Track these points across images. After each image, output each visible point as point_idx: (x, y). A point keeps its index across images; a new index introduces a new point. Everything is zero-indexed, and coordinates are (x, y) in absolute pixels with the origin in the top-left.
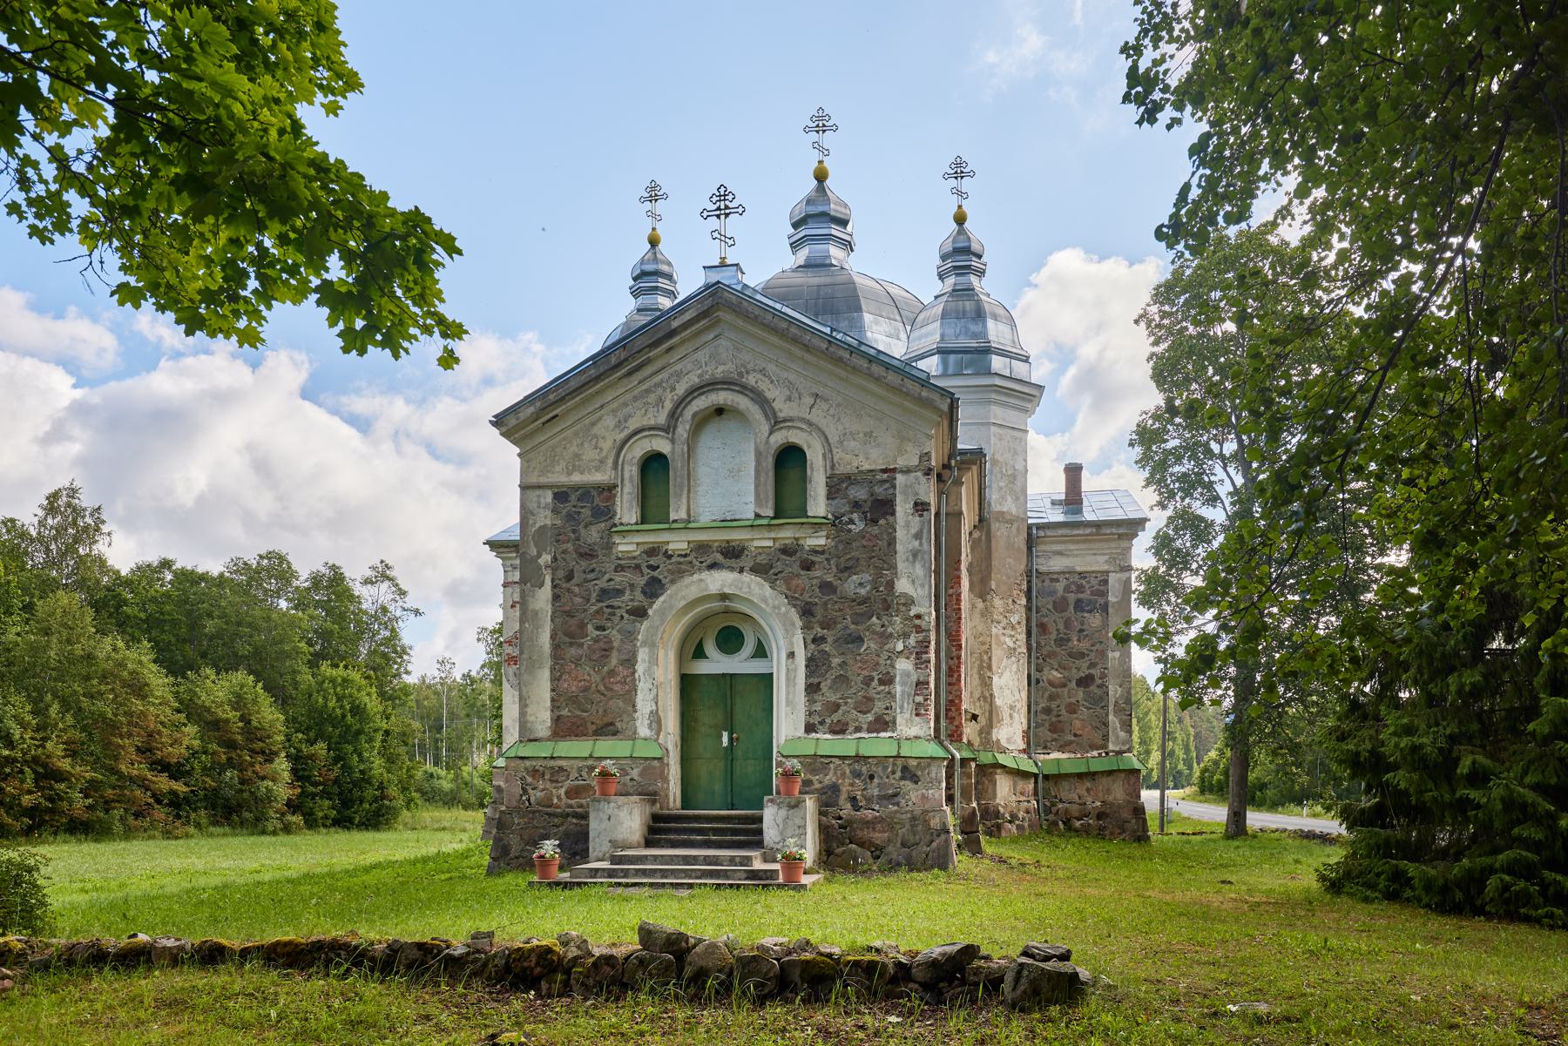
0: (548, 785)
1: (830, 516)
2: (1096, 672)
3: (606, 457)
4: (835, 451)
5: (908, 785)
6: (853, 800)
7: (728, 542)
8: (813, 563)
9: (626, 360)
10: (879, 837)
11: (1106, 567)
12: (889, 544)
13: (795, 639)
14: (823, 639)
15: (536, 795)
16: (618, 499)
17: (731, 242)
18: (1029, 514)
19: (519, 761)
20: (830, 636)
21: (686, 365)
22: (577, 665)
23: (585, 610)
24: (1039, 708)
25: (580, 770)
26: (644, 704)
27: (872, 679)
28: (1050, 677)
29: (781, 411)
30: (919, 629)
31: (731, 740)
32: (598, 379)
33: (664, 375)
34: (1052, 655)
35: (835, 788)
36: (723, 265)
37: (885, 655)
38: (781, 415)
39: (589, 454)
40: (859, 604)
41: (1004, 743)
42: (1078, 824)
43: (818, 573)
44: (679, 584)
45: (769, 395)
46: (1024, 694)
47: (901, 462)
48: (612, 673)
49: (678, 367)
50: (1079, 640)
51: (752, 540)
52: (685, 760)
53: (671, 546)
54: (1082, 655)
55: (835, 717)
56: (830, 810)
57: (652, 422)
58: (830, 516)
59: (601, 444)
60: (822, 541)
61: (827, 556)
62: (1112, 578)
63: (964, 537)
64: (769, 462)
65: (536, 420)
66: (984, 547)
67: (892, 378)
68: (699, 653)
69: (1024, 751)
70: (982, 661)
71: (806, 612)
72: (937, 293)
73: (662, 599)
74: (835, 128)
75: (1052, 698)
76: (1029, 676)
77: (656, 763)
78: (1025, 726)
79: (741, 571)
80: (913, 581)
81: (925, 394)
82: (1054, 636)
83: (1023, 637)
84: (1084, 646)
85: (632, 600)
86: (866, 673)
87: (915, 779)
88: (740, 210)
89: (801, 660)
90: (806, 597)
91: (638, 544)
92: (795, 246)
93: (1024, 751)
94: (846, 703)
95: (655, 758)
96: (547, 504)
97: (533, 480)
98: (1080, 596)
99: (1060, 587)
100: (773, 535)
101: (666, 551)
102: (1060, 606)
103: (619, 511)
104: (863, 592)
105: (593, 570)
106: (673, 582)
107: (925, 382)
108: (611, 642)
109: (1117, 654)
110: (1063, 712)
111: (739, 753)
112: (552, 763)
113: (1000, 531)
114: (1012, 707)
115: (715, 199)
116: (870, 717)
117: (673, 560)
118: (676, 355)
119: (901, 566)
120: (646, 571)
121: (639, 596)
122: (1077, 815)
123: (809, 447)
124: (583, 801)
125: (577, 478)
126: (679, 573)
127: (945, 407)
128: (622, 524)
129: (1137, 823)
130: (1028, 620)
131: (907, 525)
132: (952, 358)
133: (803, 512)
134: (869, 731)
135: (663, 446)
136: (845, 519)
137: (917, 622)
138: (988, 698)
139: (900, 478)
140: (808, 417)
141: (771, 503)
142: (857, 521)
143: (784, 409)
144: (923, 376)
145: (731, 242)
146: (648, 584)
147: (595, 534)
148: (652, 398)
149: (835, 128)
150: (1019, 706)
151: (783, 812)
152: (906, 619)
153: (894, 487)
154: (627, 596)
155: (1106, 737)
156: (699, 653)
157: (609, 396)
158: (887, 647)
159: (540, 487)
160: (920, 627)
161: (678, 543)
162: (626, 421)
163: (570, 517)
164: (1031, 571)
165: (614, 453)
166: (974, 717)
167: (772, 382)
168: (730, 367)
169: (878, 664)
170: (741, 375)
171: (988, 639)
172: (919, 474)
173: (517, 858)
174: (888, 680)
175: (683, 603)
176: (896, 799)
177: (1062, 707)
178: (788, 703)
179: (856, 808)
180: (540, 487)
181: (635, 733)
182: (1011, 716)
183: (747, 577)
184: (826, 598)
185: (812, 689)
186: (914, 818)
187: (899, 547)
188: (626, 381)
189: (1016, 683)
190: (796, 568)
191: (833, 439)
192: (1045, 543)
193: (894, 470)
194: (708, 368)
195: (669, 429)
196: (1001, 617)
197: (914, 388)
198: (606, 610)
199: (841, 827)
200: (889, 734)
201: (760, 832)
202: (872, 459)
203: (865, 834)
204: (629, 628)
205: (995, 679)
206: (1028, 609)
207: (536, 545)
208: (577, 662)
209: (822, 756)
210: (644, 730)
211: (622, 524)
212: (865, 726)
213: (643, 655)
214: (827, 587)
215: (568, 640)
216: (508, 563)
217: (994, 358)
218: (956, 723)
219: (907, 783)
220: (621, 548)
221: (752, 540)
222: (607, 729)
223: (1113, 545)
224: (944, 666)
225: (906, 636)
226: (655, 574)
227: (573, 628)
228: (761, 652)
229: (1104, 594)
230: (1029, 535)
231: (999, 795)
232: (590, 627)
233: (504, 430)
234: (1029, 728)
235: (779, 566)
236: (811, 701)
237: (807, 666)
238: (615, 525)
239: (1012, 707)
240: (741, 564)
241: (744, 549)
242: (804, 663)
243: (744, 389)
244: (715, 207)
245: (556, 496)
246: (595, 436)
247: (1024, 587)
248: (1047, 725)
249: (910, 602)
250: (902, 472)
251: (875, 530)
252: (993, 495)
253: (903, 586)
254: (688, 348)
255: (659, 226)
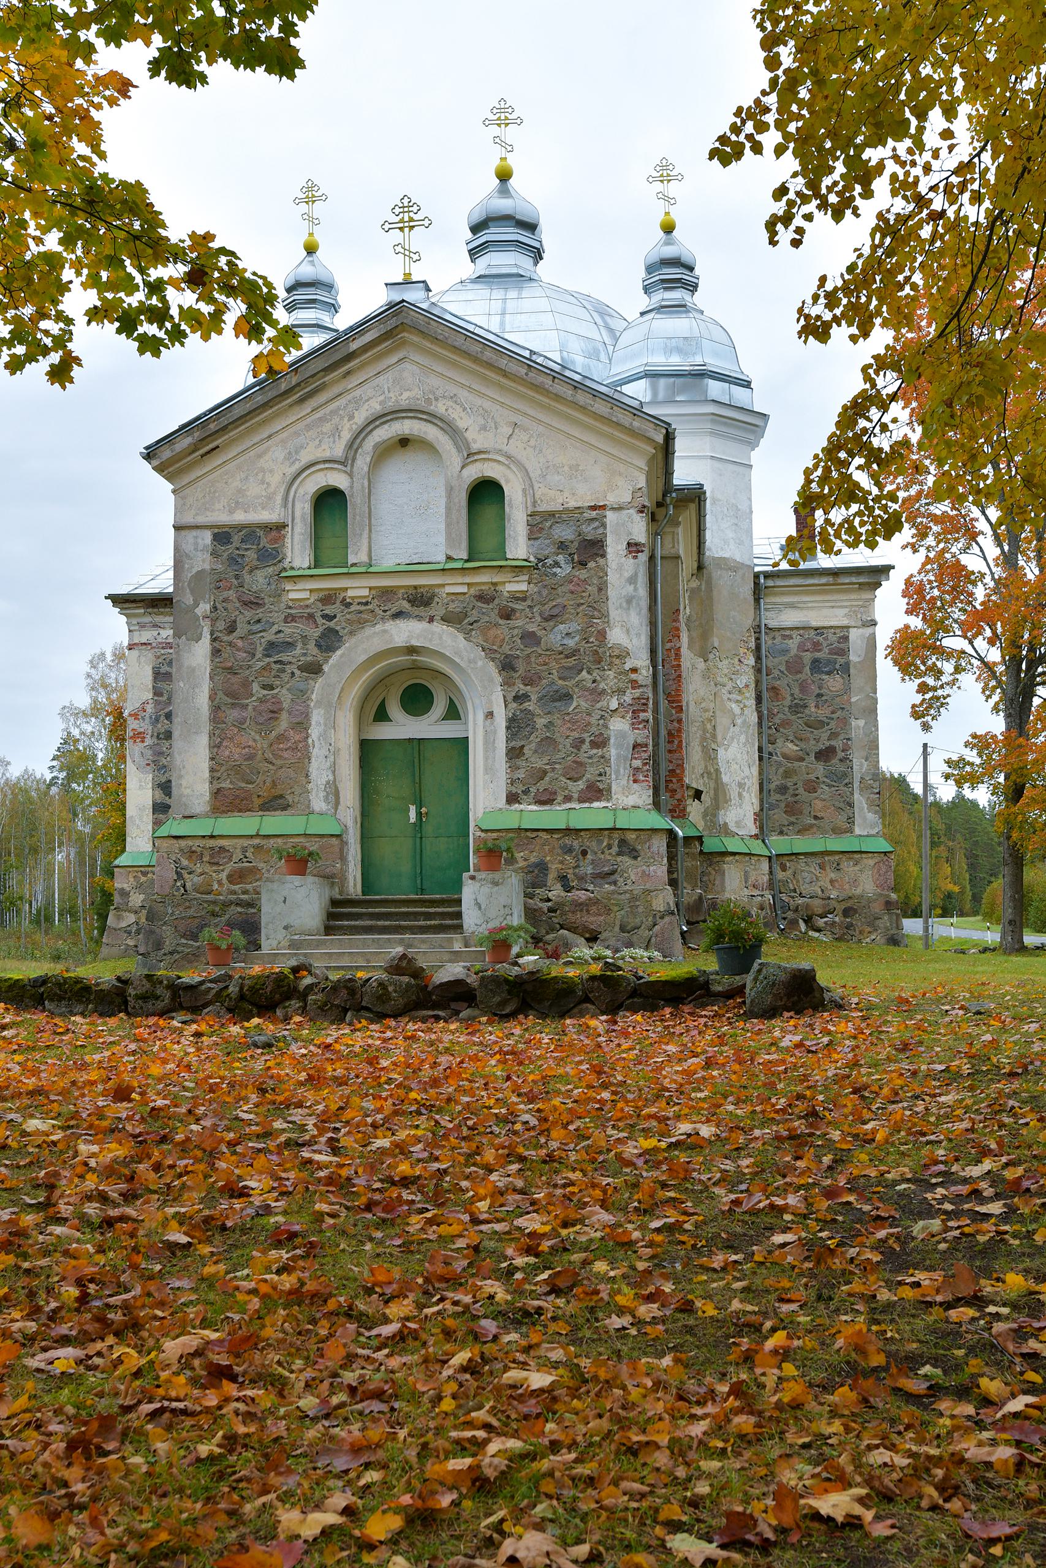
0: (208, 868)
1: (532, 559)
2: (838, 743)
3: (274, 493)
4: (536, 486)
5: (626, 860)
6: (563, 879)
7: (415, 587)
8: (513, 610)
9: (298, 385)
10: (593, 921)
11: (845, 622)
12: (600, 590)
13: (493, 698)
14: (525, 697)
15: (192, 881)
16: (288, 540)
17: (415, 257)
18: (756, 561)
19: (174, 841)
20: (534, 693)
21: (367, 390)
22: (240, 729)
23: (250, 667)
24: (773, 786)
25: (244, 850)
26: (319, 772)
27: (583, 741)
28: (785, 750)
29: (475, 441)
30: (635, 685)
31: (419, 815)
32: (266, 405)
33: (341, 402)
34: (786, 723)
35: (542, 867)
36: (408, 282)
37: (597, 715)
38: (475, 447)
39: (254, 490)
40: (567, 657)
41: (732, 827)
42: (821, 922)
43: (519, 623)
44: (359, 636)
45: (461, 424)
46: (755, 770)
47: (611, 499)
48: (281, 738)
49: (358, 393)
50: (817, 706)
51: (443, 586)
52: (366, 837)
53: (350, 593)
54: (821, 724)
55: (542, 785)
56: (538, 891)
57: (327, 454)
58: (532, 559)
59: (268, 478)
60: (523, 587)
61: (529, 602)
62: (854, 634)
63: (682, 586)
64: (462, 498)
65: (193, 452)
66: (704, 598)
67: (601, 408)
68: (381, 715)
69: (756, 837)
70: (705, 731)
71: (507, 666)
72: (643, 309)
73: (339, 652)
74: (519, 122)
75: (787, 774)
76: (760, 750)
77: (334, 840)
78: (757, 808)
79: (431, 620)
80: (628, 631)
81: (636, 424)
82: (787, 702)
83: (752, 702)
84: (823, 713)
85: (305, 654)
86: (575, 734)
87: (634, 854)
88: (426, 223)
89: (501, 722)
90: (506, 649)
91: (311, 591)
92: (474, 253)
93: (756, 837)
94: (553, 769)
95: (332, 836)
96: (205, 546)
97: (188, 519)
98: (818, 655)
99: (793, 644)
100: (468, 580)
101: (344, 599)
102: (794, 667)
103: (289, 554)
104: (571, 643)
105: (259, 621)
106: (352, 633)
107: (637, 412)
108: (280, 703)
109: (861, 723)
110: (801, 791)
111: (428, 829)
112: (212, 843)
113: (722, 581)
114: (741, 785)
115: (397, 210)
116: (581, 785)
117: (353, 608)
118: (355, 380)
119: (614, 614)
120: (320, 621)
121: (312, 649)
122: (820, 911)
123: (507, 481)
124: (249, 887)
125: (240, 517)
126: (360, 623)
127: (660, 438)
128: (292, 568)
129: (890, 920)
130: (758, 683)
131: (620, 568)
132: (662, 382)
133: (500, 551)
134: (581, 800)
135: (339, 480)
136: (549, 561)
137: (633, 676)
138: (714, 774)
139: (611, 517)
140: (505, 448)
141: (464, 544)
142: (562, 563)
143: (478, 440)
144: (635, 404)
145: (415, 257)
146: (323, 636)
147: (261, 580)
148: (327, 427)
149: (519, 122)
150: (748, 783)
151: (486, 889)
152: (621, 673)
153: (604, 525)
154: (298, 651)
155: (851, 820)
156: (381, 715)
157: (277, 425)
158: (599, 705)
159: (197, 527)
160: (636, 681)
161: (358, 589)
162: (297, 452)
163: (233, 560)
164: (759, 626)
165: (282, 490)
166: (698, 795)
167: (464, 409)
168: (416, 393)
169: (589, 724)
170: (428, 401)
171: (712, 705)
172: (632, 511)
173: (171, 953)
174: (600, 742)
175: (363, 658)
176: (613, 878)
177: (800, 784)
178: (487, 770)
179: (568, 889)
180: (197, 527)
181: (308, 807)
182: (740, 795)
183: (438, 627)
184: (529, 650)
185: (514, 754)
186: (634, 898)
187: (611, 592)
188: (296, 408)
189: (745, 757)
190: (494, 617)
191: (535, 470)
192: (775, 594)
193: (603, 507)
194: (392, 395)
195: (345, 462)
196: (725, 680)
197: (626, 419)
198: (274, 666)
199: (550, 910)
200: (603, 804)
201: (459, 915)
202: (580, 495)
203: (580, 918)
204: (302, 686)
205: (721, 752)
206: (758, 670)
207: (192, 592)
208: (240, 724)
209: (527, 830)
210: (319, 803)
211: (292, 568)
212: (576, 796)
213: (317, 717)
214: (530, 638)
215: (230, 701)
216: (134, 621)
217: (711, 383)
218: (678, 796)
219: (625, 859)
220: (292, 595)
221: (443, 586)
222: (275, 803)
223: (853, 596)
224: (663, 733)
225: (621, 692)
226: (332, 624)
227: (236, 687)
228: (453, 713)
229: (844, 652)
230: (756, 584)
231: (728, 888)
232: (255, 687)
233: (156, 462)
234: (762, 810)
235: (474, 615)
236: (513, 768)
237: (508, 728)
238: (285, 570)
239: (741, 785)
240: (432, 613)
241: (433, 596)
242: (504, 724)
243: (431, 418)
244: (397, 219)
245: (216, 537)
246: (263, 470)
247: (752, 645)
248: (783, 805)
249: (623, 654)
250: (613, 509)
251: (583, 574)
252: (711, 537)
253: (616, 636)
254: (371, 371)
255: (316, 230)
